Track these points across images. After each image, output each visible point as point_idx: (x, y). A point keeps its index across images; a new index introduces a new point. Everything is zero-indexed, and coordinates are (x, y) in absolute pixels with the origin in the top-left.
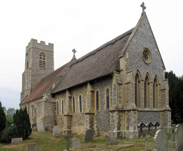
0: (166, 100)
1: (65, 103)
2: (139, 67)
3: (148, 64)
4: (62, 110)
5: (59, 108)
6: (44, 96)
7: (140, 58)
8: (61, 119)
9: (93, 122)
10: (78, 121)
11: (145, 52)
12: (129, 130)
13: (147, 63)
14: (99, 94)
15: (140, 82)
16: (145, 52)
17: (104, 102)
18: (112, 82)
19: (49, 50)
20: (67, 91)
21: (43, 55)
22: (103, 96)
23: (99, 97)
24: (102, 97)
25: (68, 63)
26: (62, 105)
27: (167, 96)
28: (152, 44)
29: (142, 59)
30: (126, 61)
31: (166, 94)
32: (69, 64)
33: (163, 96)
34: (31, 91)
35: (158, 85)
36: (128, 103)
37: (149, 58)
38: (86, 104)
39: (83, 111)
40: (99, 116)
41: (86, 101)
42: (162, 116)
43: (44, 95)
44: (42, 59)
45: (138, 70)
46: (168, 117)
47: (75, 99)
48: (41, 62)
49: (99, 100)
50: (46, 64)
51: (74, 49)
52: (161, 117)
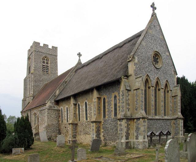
0: (178, 107)
1: (70, 110)
2: (149, 72)
3: (158, 69)
4: (66, 118)
5: (63, 116)
6: (47, 103)
7: (150, 62)
8: (65, 127)
9: (100, 130)
10: (84, 130)
11: (156, 56)
12: (138, 139)
13: (158, 68)
14: (106, 100)
15: (150, 88)
16: (156, 56)
17: (111, 109)
18: (119, 88)
19: (53, 54)
20: (71, 97)
21: (46, 59)
22: (111, 103)
23: (106, 104)
24: (110, 104)
25: (72, 68)
26: (66, 113)
27: (179, 103)
28: (163, 47)
29: (152, 63)
30: (134, 65)
31: (178, 101)
32: (74, 68)
33: (175, 103)
34: (34, 98)
35: (170, 92)
36: (138, 111)
37: (159, 62)
38: (92, 111)
39: (89, 119)
40: (106, 125)
41: (92, 109)
42: (174, 125)
43: (47, 102)
44: (45, 63)
45: (147, 75)
46: (180, 125)
47: (80, 106)
48: (43, 66)
49: (106, 107)
50: (49, 68)
51: (79, 53)
52: (173, 125)
